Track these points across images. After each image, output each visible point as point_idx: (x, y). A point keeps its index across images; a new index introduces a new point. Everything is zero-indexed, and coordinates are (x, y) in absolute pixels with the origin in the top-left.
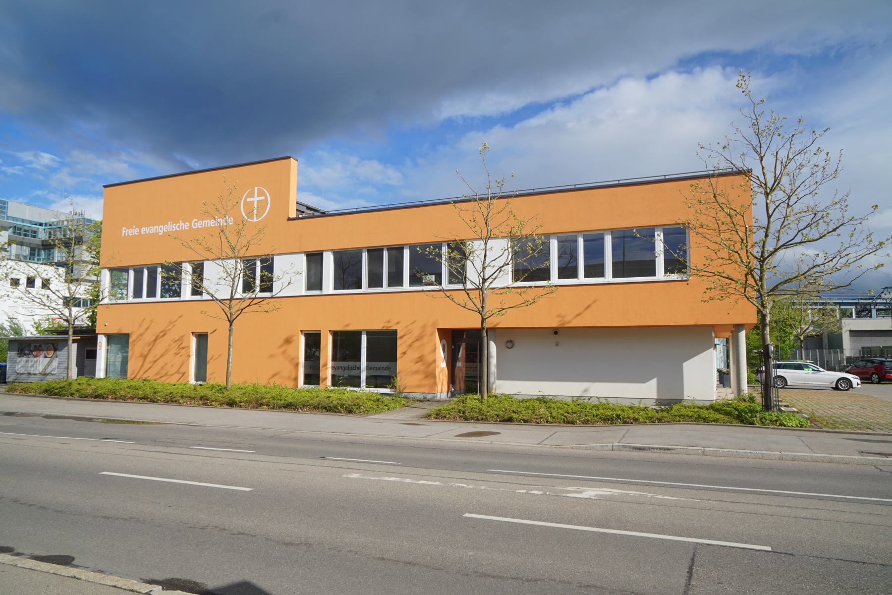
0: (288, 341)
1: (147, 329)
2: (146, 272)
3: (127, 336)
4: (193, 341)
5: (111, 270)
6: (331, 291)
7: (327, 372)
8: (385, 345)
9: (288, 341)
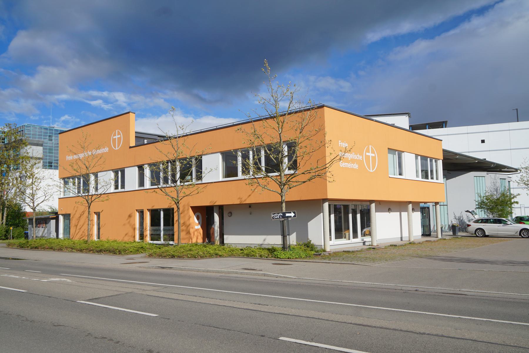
0: (130, 216)
2: (120, 173)
3: (69, 215)
4: (137, 215)
7: (148, 233)
9: (130, 216)
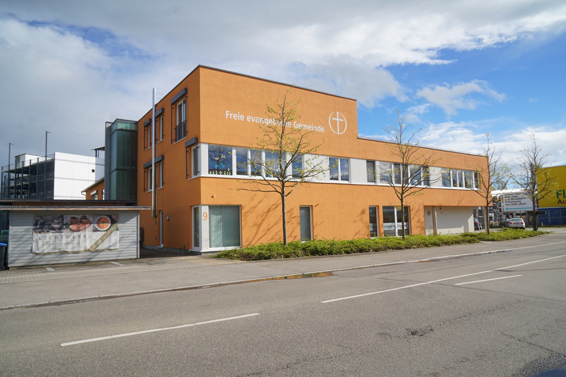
5: (395, 164)
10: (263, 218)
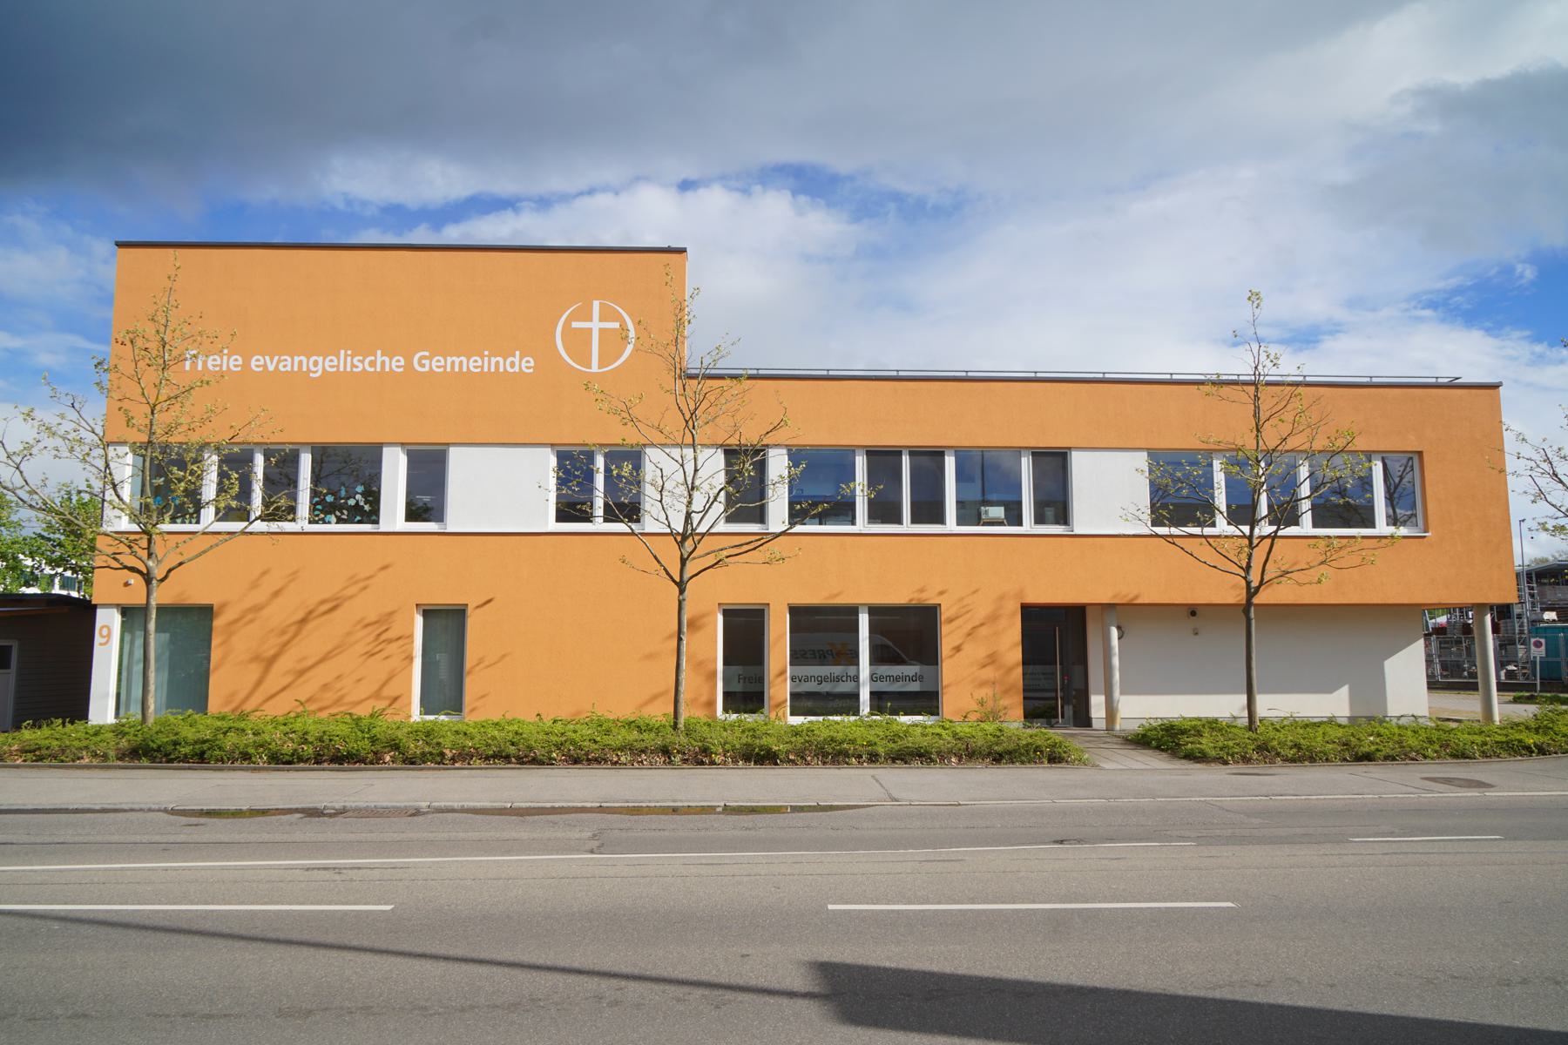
1: (277, 594)
6: (401, 524)
8: (910, 634)
10: (286, 638)
